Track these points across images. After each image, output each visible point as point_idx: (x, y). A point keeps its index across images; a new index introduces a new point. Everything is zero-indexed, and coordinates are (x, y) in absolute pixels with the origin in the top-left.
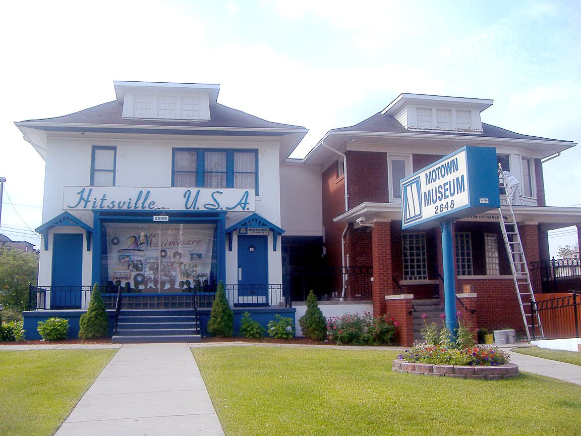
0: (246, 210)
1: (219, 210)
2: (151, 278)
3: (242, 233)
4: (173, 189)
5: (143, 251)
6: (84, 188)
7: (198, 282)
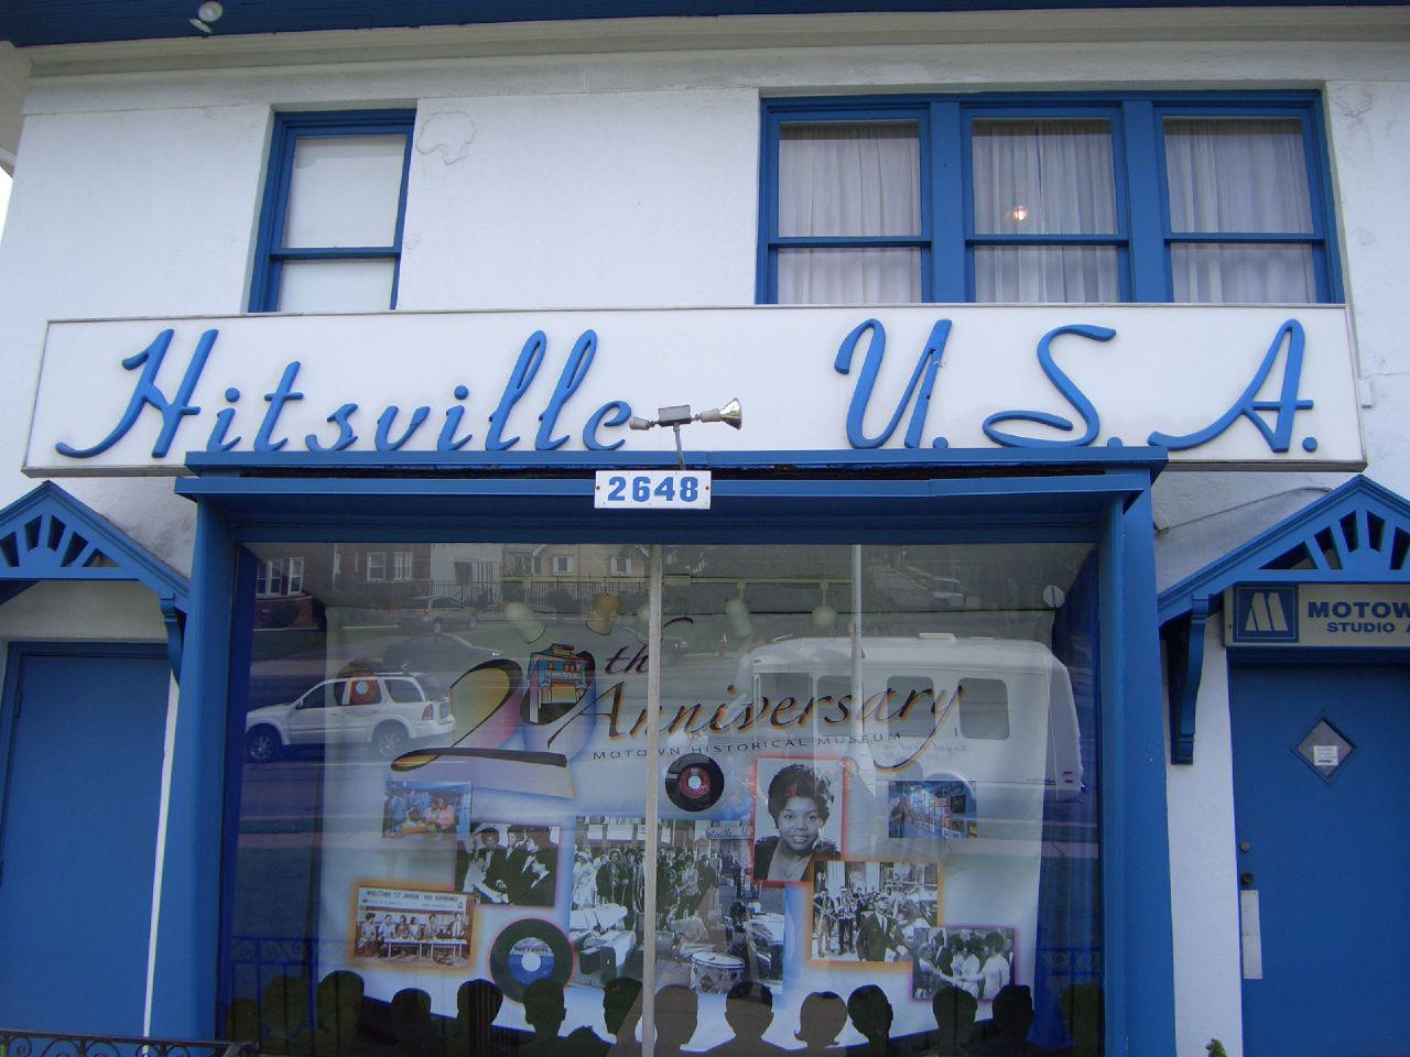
0: (1296, 453)
1: (1101, 442)
2: (610, 953)
3: (1258, 634)
4: (768, 316)
5: (560, 760)
6: (167, 326)
7: (951, 1002)
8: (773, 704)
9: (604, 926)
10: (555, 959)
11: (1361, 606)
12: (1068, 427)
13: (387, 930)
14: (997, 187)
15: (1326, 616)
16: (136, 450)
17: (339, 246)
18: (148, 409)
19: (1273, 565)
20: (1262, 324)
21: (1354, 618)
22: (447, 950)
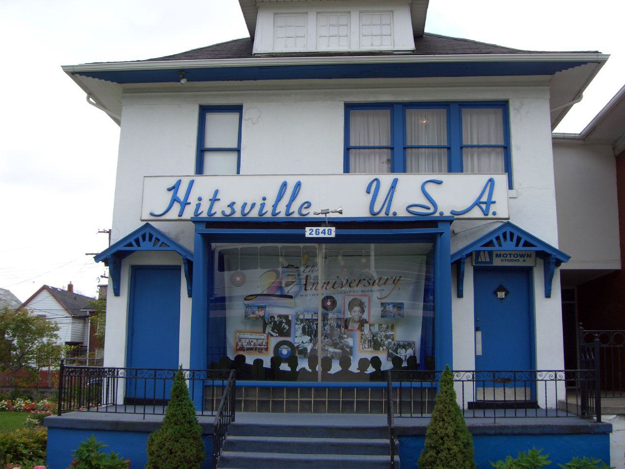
0: (490, 216)
1: (437, 214)
2: (306, 349)
3: (482, 262)
5: (291, 297)
6: (179, 178)
8: (349, 282)
9: (304, 342)
10: (291, 350)
11: (510, 255)
12: (428, 208)
13: (245, 344)
14: (413, 132)
15: (501, 257)
16: (174, 214)
17: (222, 147)
18: (176, 202)
19: (483, 246)
20: (481, 180)
21: (508, 258)
22: (262, 349)
